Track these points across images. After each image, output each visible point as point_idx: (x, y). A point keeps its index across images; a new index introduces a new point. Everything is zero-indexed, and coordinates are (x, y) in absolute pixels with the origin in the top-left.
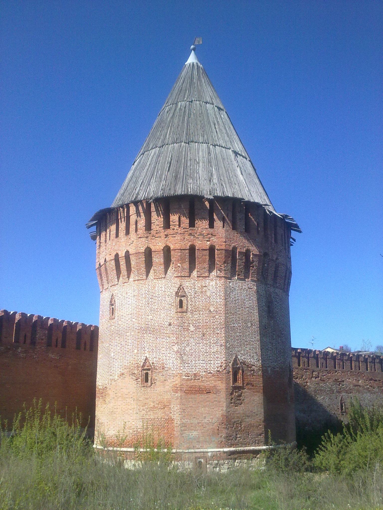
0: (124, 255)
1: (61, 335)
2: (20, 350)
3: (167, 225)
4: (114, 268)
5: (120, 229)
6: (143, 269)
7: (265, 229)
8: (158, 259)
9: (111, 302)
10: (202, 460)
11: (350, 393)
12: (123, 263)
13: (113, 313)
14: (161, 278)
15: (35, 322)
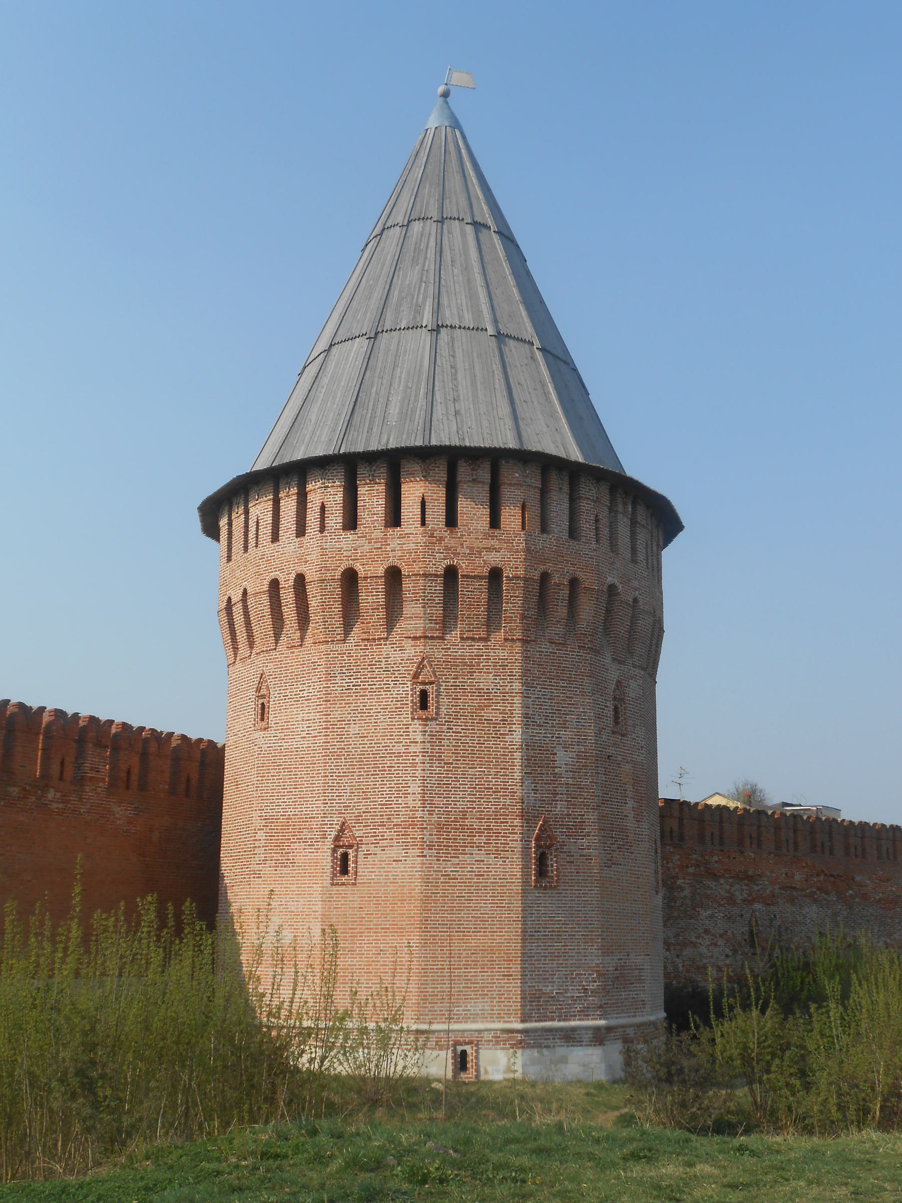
0: (291, 582)
1: (135, 760)
2: (51, 795)
3: (394, 518)
4: (267, 611)
5: (282, 521)
6: (337, 621)
7: (613, 526)
8: (372, 597)
9: (258, 690)
10: (469, 1051)
11: (773, 905)
12: (288, 597)
13: (263, 714)
14: (379, 639)
15: (11, 714)
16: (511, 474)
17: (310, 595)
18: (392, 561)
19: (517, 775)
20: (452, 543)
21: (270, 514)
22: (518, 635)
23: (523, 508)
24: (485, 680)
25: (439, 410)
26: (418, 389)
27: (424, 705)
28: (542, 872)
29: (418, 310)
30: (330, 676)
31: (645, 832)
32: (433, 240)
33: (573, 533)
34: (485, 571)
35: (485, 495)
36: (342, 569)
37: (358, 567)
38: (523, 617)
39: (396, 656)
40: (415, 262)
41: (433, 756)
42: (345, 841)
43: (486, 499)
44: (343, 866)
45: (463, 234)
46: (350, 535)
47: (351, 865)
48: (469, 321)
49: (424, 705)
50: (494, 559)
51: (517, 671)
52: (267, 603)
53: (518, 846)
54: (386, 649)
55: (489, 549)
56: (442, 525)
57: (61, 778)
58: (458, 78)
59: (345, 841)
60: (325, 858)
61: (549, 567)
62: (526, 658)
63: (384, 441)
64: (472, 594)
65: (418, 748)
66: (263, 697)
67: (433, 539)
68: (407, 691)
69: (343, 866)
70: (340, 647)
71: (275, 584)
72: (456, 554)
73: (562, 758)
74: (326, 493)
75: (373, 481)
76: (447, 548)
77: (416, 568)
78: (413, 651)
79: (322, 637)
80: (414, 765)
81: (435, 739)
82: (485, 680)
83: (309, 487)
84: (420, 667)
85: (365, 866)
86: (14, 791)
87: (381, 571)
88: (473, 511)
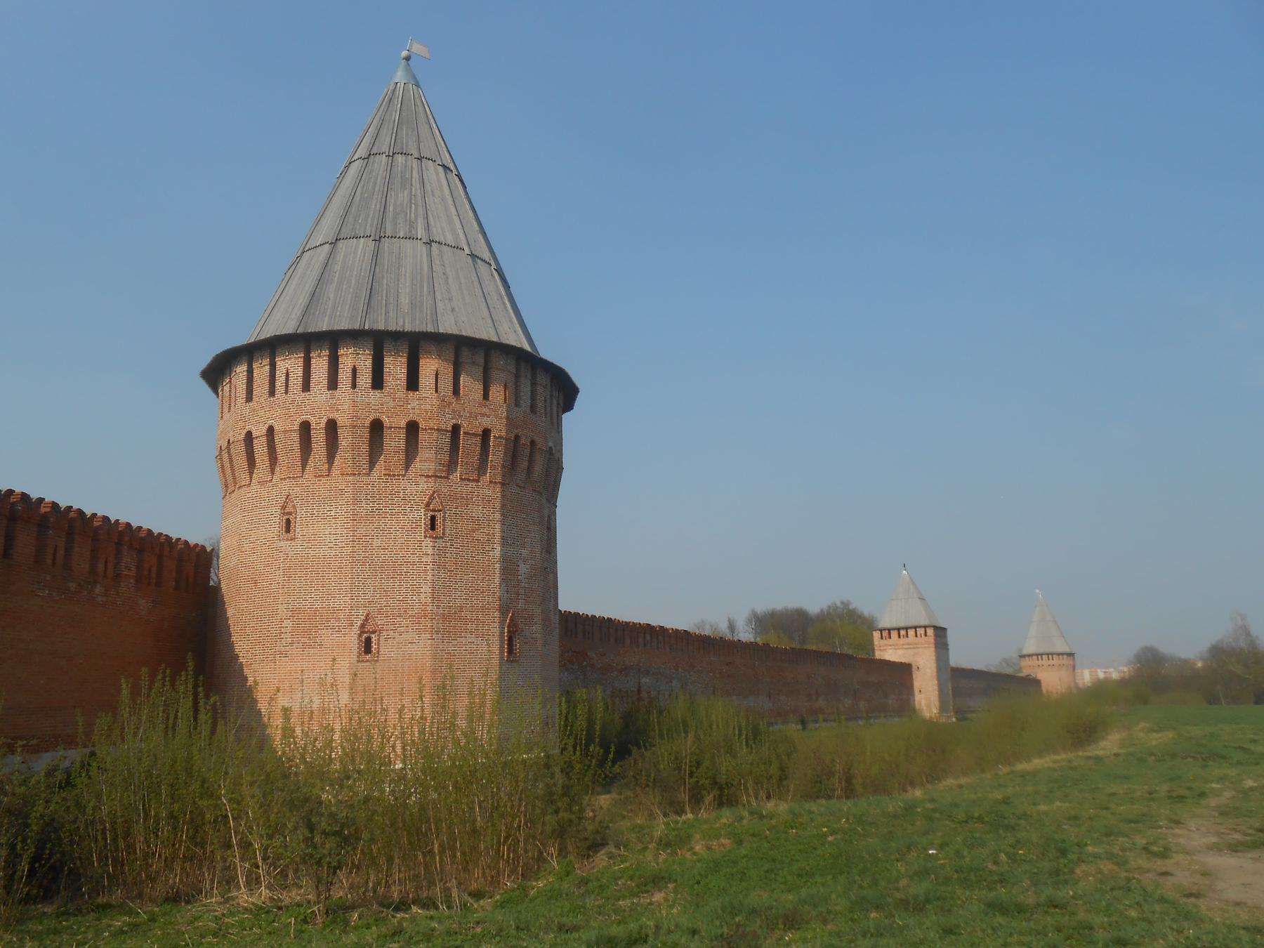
0: (323, 425)
3: (413, 383)
8: (394, 442)
12: (260, 447)
16: (499, 361)
17: (341, 437)
18: (411, 417)
19: (497, 580)
20: (457, 407)
21: (301, 369)
22: (499, 479)
23: (505, 387)
24: (477, 511)
25: (440, 305)
26: (422, 287)
27: (433, 527)
28: (510, 651)
29: (412, 225)
30: (356, 501)
31: (556, 619)
32: (415, 172)
33: (533, 408)
34: (480, 431)
35: (480, 375)
36: (371, 418)
37: (384, 418)
38: (503, 466)
39: (411, 488)
40: (403, 186)
41: (439, 566)
42: (368, 628)
43: (481, 377)
44: (367, 647)
45: (437, 174)
46: (377, 393)
47: (374, 646)
48: (450, 241)
49: (433, 527)
50: (486, 422)
51: (498, 506)
52: (297, 439)
53: (497, 631)
54: (403, 483)
55: (483, 415)
56: (450, 393)
57: (105, 576)
58: (417, 48)
59: (368, 628)
60: (352, 639)
61: (519, 431)
62: (503, 496)
63: (401, 323)
64: (469, 446)
65: (429, 559)
66: (290, 514)
67: (444, 403)
68: (421, 515)
69: (367, 647)
70: (365, 479)
71: (305, 427)
72: (461, 417)
73: (523, 568)
74: (355, 359)
75: (397, 354)
76: (454, 411)
77: (432, 424)
78: (425, 486)
79: (350, 470)
80: (426, 571)
81: (441, 553)
82: (477, 511)
83: (341, 352)
84: (432, 498)
85: (386, 648)
86: (72, 586)
87: (403, 424)
88: (470, 385)
